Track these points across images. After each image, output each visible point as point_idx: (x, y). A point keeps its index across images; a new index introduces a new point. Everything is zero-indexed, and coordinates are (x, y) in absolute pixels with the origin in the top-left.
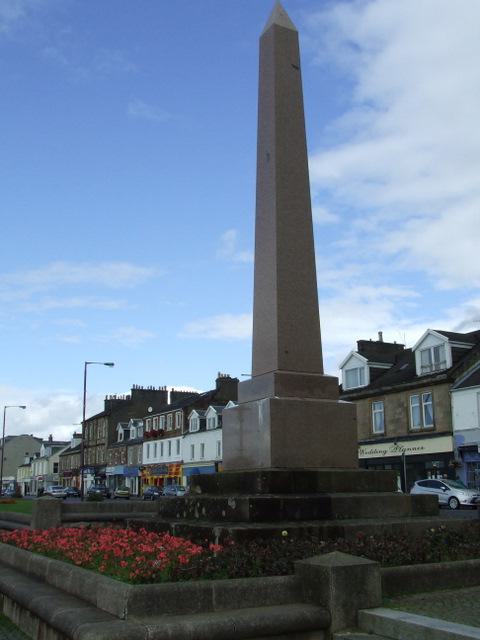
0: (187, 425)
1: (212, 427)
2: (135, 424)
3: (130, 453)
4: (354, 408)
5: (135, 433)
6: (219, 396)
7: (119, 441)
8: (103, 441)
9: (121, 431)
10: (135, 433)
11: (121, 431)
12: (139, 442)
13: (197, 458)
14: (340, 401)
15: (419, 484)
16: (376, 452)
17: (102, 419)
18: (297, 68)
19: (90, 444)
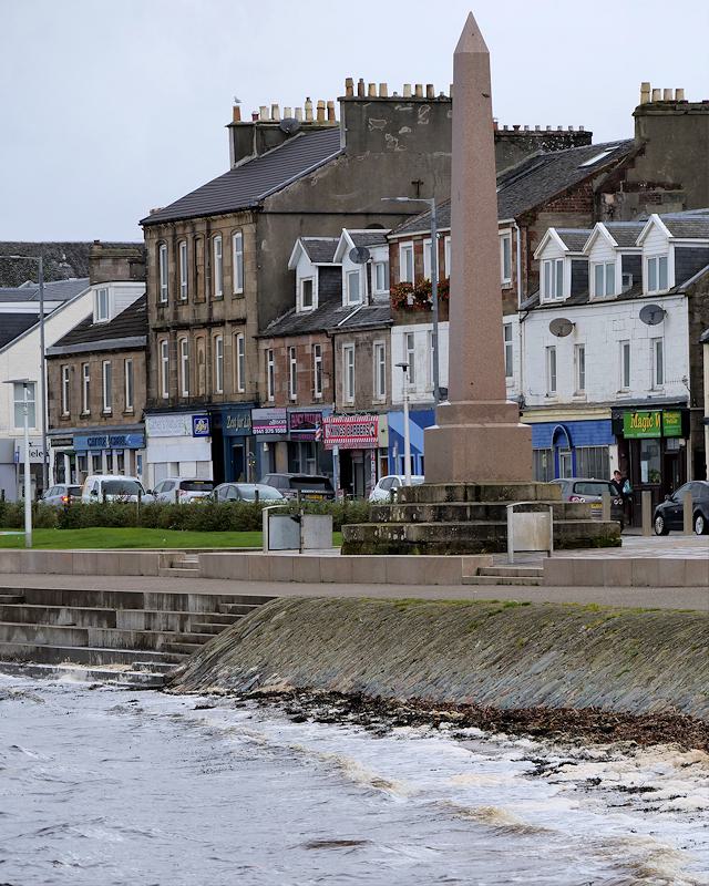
0: (532, 277)
1: (604, 297)
2: (361, 254)
3: (345, 365)
4: (115, 612)
5: (361, 289)
6: (642, 172)
7: (300, 307)
8: (238, 310)
9: (307, 270)
10: (361, 289)
11: (307, 270)
12: (373, 326)
13: (565, 394)
14: (520, 425)
15: (517, 509)
16: (68, 569)
17: (232, 221)
18: (488, 96)
19: (186, 315)
